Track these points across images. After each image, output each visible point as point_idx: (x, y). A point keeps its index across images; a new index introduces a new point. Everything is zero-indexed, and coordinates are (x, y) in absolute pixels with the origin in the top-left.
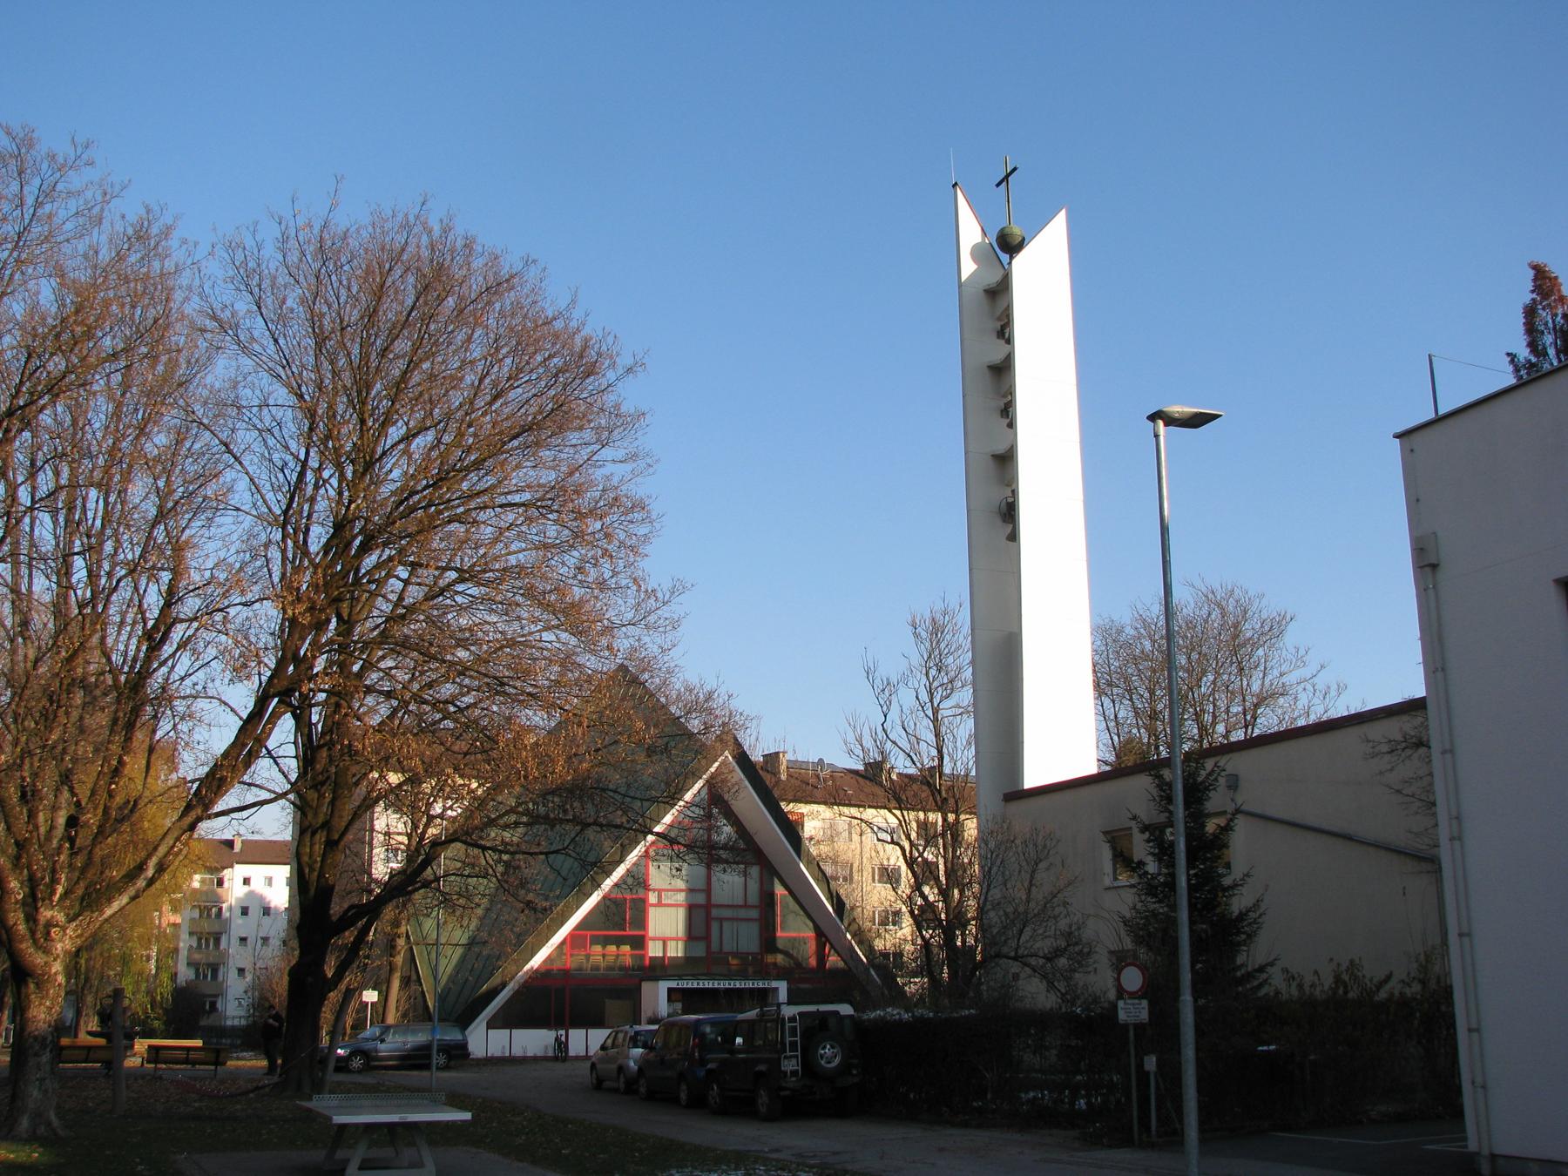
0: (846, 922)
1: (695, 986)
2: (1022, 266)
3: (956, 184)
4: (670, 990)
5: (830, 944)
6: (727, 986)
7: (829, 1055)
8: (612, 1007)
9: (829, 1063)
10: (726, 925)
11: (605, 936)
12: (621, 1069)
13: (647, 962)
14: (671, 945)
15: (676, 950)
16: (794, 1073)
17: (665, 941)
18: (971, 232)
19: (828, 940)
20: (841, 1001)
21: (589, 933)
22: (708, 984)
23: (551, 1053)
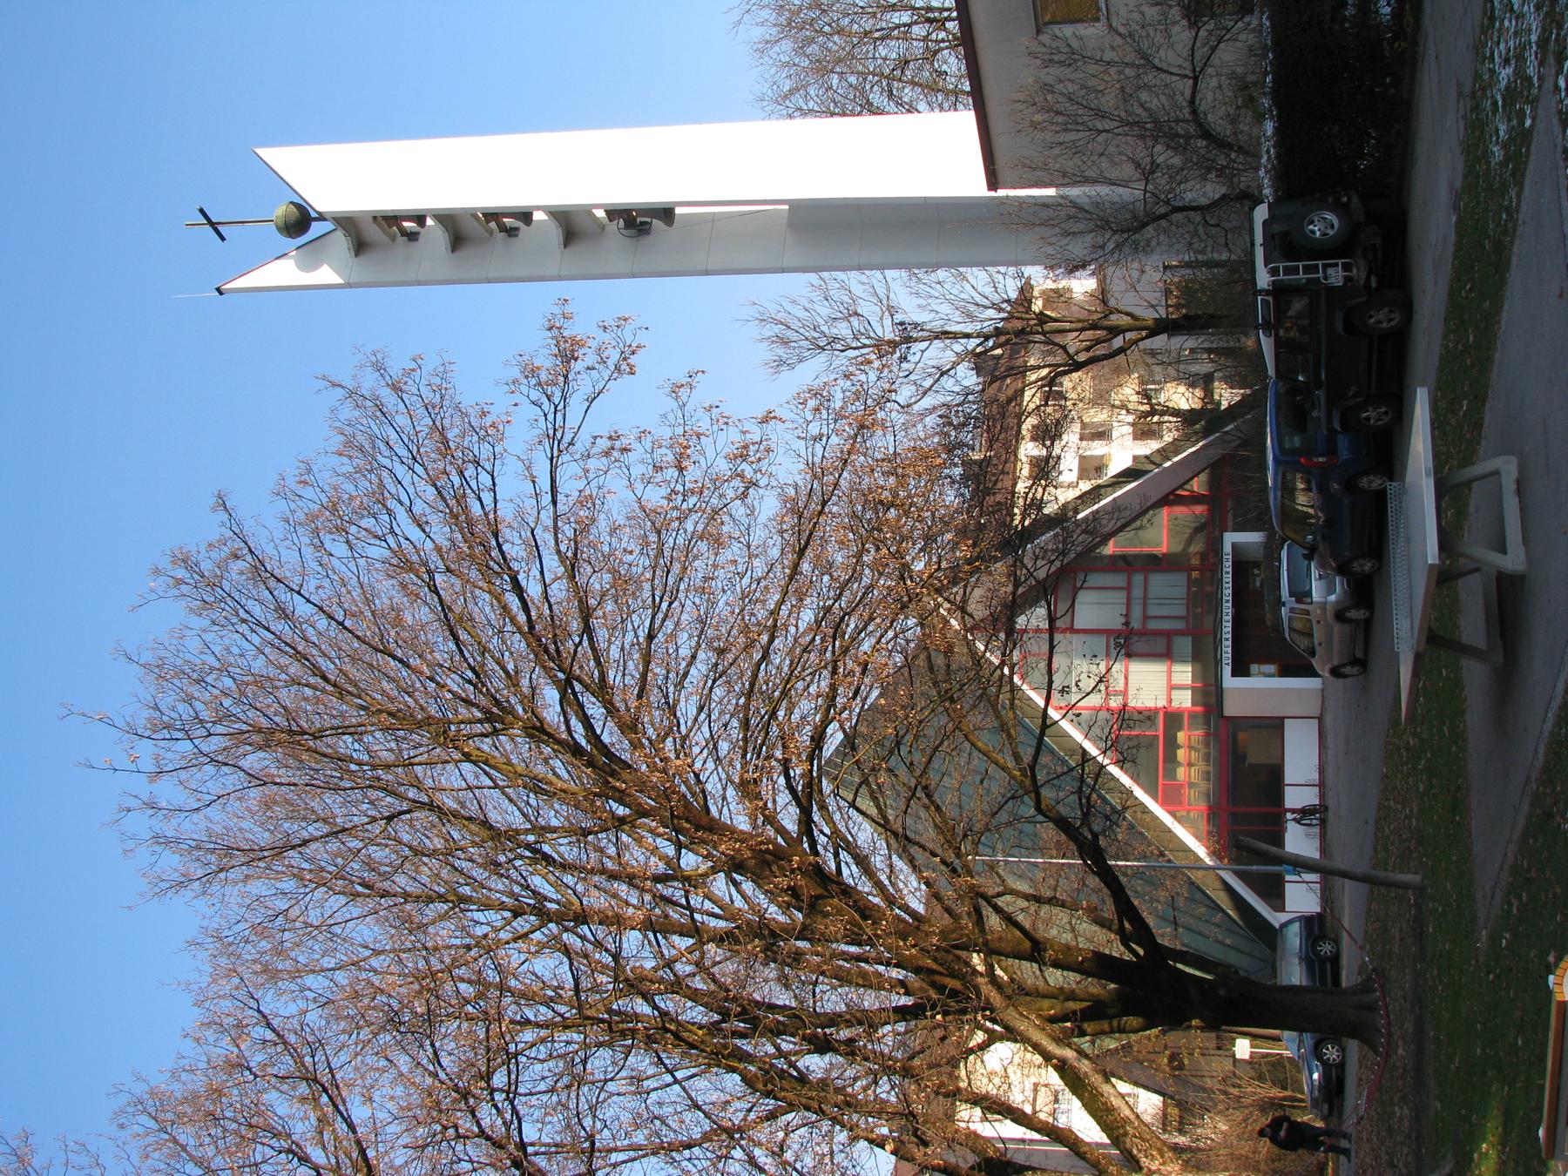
0: (1150, 467)
1: (1229, 643)
2: (325, 199)
3: (218, 290)
4: (1234, 674)
5: (1177, 489)
6: (1230, 604)
7: (1323, 225)
8: (1255, 756)
9: (1332, 226)
10: (1152, 611)
11: (1164, 762)
12: (1340, 616)
13: (1199, 709)
14: (1177, 679)
15: (1184, 673)
16: (1346, 267)
17: (1172, 687)
18: (283, 272)
19: (1172, 492)
20: (1251, 221)
21: (1161, 781)
22: (1227, 627)
23: (1317, 830)
